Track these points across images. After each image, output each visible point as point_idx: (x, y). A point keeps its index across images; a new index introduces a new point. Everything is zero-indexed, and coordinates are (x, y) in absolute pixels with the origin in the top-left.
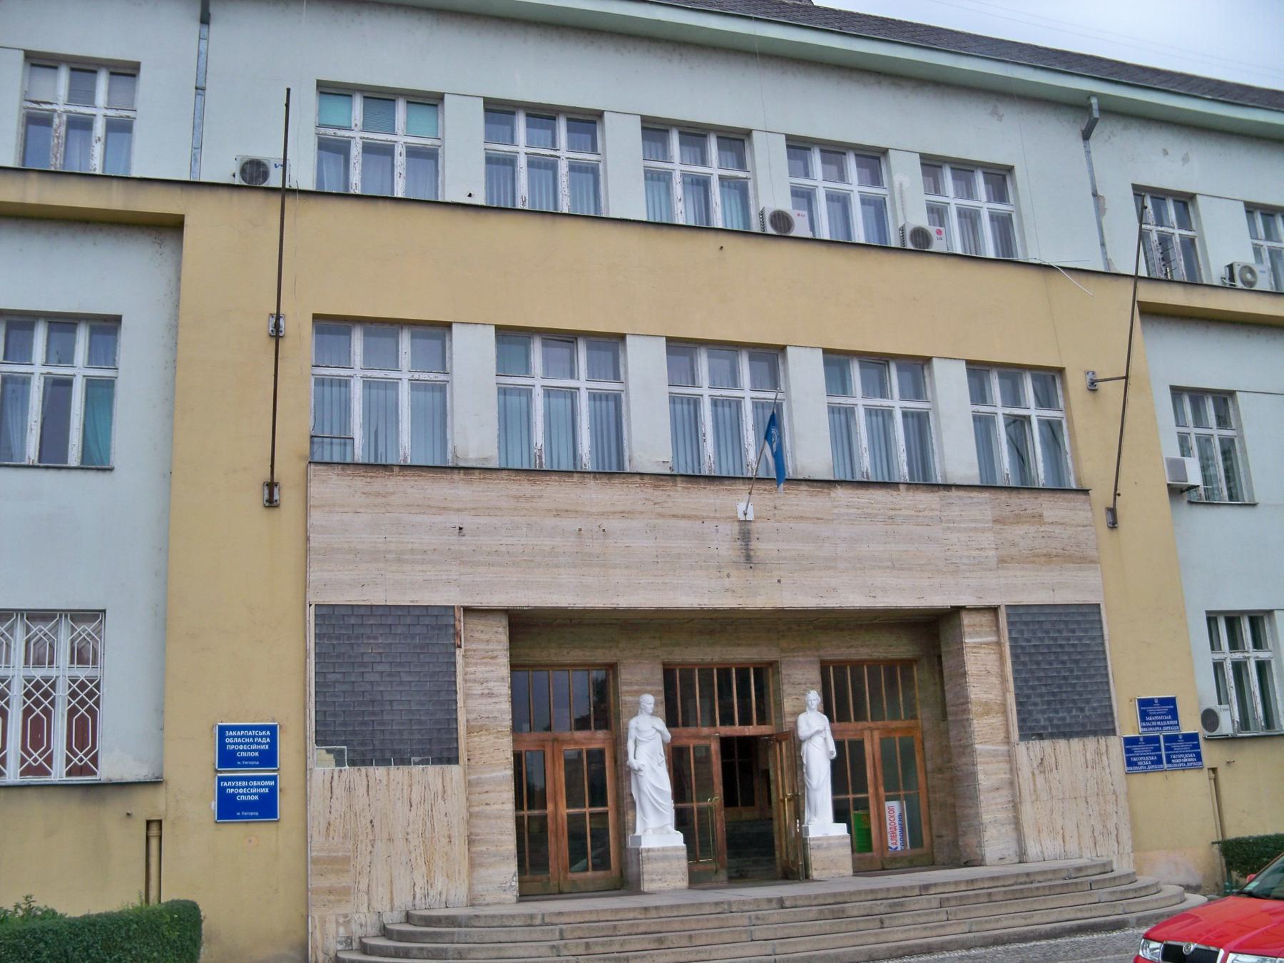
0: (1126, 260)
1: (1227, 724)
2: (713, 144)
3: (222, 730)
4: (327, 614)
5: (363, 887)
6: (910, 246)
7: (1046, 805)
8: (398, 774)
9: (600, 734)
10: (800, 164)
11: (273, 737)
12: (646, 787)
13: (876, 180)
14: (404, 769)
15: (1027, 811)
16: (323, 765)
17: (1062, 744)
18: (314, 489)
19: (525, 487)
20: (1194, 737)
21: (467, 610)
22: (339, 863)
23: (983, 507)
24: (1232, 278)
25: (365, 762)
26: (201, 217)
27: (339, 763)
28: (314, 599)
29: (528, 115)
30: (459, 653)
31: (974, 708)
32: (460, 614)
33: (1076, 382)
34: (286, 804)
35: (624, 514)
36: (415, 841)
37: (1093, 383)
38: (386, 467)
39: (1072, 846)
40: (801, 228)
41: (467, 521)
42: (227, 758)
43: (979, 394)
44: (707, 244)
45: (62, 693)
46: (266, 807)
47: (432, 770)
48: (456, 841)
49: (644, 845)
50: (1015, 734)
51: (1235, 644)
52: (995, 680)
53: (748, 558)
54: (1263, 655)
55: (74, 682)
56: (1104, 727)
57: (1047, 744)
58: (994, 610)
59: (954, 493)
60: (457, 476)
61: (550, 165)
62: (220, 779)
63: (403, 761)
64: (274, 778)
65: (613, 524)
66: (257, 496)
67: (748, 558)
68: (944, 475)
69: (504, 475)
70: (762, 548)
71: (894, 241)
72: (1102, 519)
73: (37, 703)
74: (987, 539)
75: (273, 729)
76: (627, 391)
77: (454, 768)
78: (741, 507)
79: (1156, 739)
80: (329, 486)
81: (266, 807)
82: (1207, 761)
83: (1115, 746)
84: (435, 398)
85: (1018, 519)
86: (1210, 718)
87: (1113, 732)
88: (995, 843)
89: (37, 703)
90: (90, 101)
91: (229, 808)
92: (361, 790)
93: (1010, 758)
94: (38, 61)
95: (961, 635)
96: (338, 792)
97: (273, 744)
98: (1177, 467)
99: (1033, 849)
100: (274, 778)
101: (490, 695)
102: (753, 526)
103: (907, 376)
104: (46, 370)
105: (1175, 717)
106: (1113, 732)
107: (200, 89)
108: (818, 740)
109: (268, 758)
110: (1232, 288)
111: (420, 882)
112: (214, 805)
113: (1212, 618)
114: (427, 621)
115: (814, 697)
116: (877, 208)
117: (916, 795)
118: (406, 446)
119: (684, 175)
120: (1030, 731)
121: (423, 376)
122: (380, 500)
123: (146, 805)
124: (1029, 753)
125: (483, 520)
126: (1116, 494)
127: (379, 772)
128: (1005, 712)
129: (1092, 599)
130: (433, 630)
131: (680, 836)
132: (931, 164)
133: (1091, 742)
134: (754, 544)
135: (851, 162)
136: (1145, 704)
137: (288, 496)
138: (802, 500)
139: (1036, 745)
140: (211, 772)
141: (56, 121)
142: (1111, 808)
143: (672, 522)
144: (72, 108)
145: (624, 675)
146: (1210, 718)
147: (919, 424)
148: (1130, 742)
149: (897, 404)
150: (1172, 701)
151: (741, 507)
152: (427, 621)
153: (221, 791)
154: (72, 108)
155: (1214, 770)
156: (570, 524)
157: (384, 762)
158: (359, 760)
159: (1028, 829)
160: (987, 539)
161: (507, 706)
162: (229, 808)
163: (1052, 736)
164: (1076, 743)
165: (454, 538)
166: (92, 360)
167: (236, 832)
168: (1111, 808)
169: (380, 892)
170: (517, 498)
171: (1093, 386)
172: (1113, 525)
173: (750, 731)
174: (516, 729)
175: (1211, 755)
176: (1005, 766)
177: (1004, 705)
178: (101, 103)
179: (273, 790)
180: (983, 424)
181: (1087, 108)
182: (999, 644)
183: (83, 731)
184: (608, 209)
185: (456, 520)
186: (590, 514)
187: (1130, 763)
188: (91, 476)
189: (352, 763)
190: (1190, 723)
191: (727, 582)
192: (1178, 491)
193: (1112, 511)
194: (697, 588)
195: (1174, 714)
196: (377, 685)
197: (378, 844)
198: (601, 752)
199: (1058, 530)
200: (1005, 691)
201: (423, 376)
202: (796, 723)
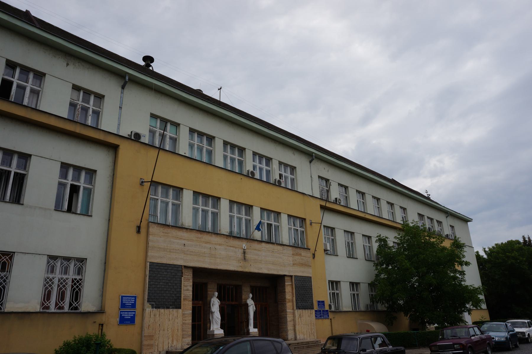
0: (317, 195)
1: (333, 309)
2: (31, 76)
3: (122, 297)
4: (153, 265)
5: (156, 344)
6: (133, 138)
7: (302, 325)
8: (167, 311)
9: (201, 302)
10: (38, 82)
11: (135, 300)
12: (215, 317)
13: (210, 145)
14: (168, 310)
15: (297, 327)
16: (148, 309)
17: (304, 310)
18: (151, 230)
19: (199, 235)
20: (327, 311)
21: (185, 267)
22: (151, 337)
23: (290, 251)
24: (336, 201)
25: (159, 308)
26: (126, 150)
27: (153, 308)
28: (150, 260)
29: (95, 96)
30: (183, 278)
31: (287, 301)
32: (183, 267)
33: (308, 222)
34: (137, 320)
35: (220, 245)
36: (170, 331)
37: (311, 223)
38: (218, 234)
39: (305, 336)
40: (257, 176)
41: (186, 242)
42: (123, 305)
43: (195, 201)
44: (240, 177)
45: (56, 281)
46: (132, 320)
47: (175, 310)
48: (179, 331)
49: (215, 333)
50: (295, 308)
51: (333, 289)
52: (291, 294)
53: (245, 259)
54: (338, 292)
55: (48, 278)
56: (312, 308)
57: (301, 310)
58: (291, 276)
59: (285, 247)
60: (184, 230)
61: (24, 88)
62: (121, 312)
63: (168, 308)
64: (135, 312)
65: (218, 247)
66: (134, 230)
67: (245, 259)
68: (282, 242)
69: (194, 231)
70: (248, 256)
71: (245, 173)
72: (311, 255)
73: (61, 283)
74: (291, 259)
75: (135, 297)
76: (220, 212)
77: (180, 310)
78: (244, 245)
79: (320, 311)
80: (153, 229)
81: (132, 320)
82: (330, 317)
83: (314, 311)
84: (177, 208)
85: (297, 254)
86: (330, 306)
87: (313, 308)
88: (291, 335)
89: (61, 283)
90: (88, 103)
91: (123, 321)
92: (158, 316)
93: (294, 313)
94: (76, 88)
95: (285, 282)
96: (152, 316)
97: (135, 302)
98: (325, 245)
99: (298, 337)
100: (135, 312)
101: (188, 290)
102: (246, 251)
103: (204, 200)
104: (72, 183)
105: (324, 306)
106: (313, 308)
107: (121, 108)
108: (252, 306)
109: (134, 306)
110: (336, 203)
111: (170, 342)
112: (118, 319)
113: (329, 281)
114: (175, 269)
115: (216, 294)
116: (268, 172)
117: (272, 322)
118: (170, 220)
119: (207, 149)
120: (298, 308)
121: (175, 202)
122: (166, 234)
123: (100, 319)
124: (298, 312)
125: (189, 243)
126: (315, 251)
127: (162, 311)
128: (293, 302)
129: (310, 275)
130: (177, 270)
131: (223, 331)
132: (226, 143)
133: (309, 311)
134: (246, 255)
135: (205, 138)
136: (319, 302)
137: (143, 230)
138: (256, 245)
139: (300, 311)
140: (118, 309)
141: (78, 107)
142: (313, 327)
143: (230, 248)
144: (83, 104)
145: (209, 286)
146: (330, 306)
147: (215, 216)
148: (316, 311)
149: (210, 209)
150: (323, 302)
151: (244, 245)
152: (175, 269)
153: (121, 315)
154: (83, 104)
155: (331, 319)
156: (208, 246)
157: (164, 308)
158: (157, 307)
159: (297, 332)
160: (291, 259)
161: (191, 293)
162: (123, 321)
163: (302, 309)
164: (306, 311)
165: (183, 247)
166: (18, 167)
167: (123, 328)
168: (313, 327)
169: (160, 345)
170: (197, 238)
171: (311, 224)
172: (314, 257)
173: (233, 303)
174: (193, 300)
175: (331, 316)
176: (292, 316)
177: (293, 300)
178: (170, 131)
179: (134, 315)
180: (231, 217)
181: (312, 156)
182: (292, 285)
183: (76, 295)
184: (39, 106)
185: (183, 242)
186: (213, 244)
187: (316, 317)
188: (86, 218)
189: (156, 308)
190: (327, 308)
191: (240, 264)
192: (325, 250)
193: (314, 255)
194: (233, 265)
195: (324, 305)
196: (162, 285)
197: (161, 331)
198: (201, 307)
199: (304, 258)
200: (293, 297)
201: (175, 202)
202: (246, 302)
